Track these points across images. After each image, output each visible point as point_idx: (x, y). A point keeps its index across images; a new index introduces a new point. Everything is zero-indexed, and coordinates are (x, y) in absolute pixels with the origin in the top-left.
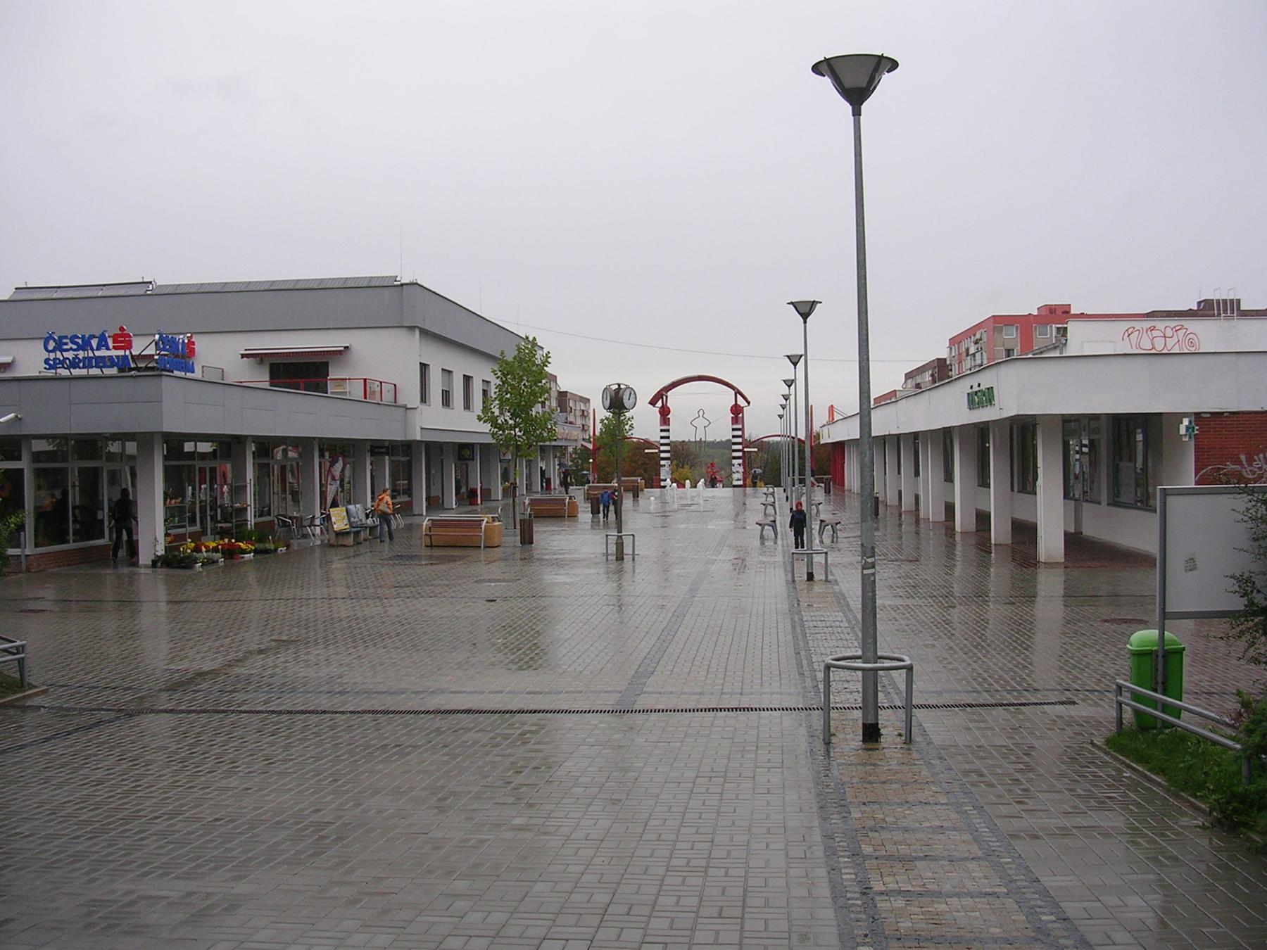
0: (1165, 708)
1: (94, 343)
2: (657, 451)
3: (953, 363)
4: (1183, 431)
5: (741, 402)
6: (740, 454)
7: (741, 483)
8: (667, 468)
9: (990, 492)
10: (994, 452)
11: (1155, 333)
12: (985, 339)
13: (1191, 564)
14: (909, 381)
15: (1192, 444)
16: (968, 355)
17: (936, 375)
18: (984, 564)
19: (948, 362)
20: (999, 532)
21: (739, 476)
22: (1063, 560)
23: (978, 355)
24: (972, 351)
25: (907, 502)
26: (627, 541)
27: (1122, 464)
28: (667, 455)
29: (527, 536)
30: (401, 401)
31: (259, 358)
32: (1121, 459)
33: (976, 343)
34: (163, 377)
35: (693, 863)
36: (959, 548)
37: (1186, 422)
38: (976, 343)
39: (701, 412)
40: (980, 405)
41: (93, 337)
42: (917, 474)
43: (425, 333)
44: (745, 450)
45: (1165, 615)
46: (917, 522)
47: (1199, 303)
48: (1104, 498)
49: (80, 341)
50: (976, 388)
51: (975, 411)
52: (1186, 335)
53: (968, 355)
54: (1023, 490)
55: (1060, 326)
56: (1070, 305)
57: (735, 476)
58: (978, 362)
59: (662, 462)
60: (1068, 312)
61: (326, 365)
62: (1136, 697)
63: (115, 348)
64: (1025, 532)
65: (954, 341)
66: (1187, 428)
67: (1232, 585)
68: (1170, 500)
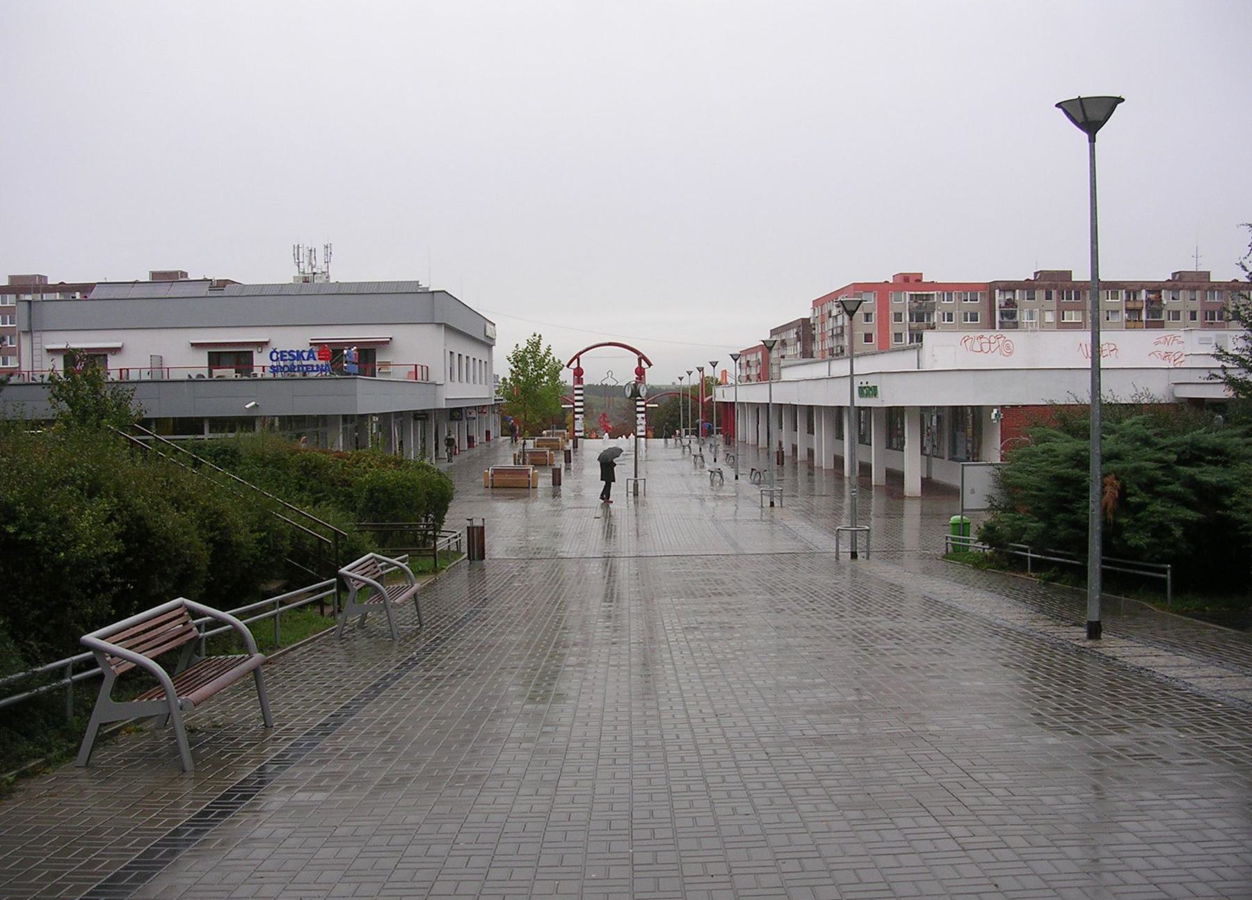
0: (964, 541)
1: (305, 355)
2: (572, 406)
3: (816, 323)
4: (993, 417)
5: (644, 364)
6: (643, 409)
7: (644, 434)
8: (580, 421)
9: (871, 449)
10: (875, 421)
11: (983, 340)
13: (973, 491)
15: (999, 424)
16: (830, 317)
17: (800, 333)
19: (812, 322)
20: (877, 477)
22: (920, 495)
25: (802, 454)
26: (641, 483)
27: (958, 433)
28: (581, 410)
29: (557, 480)
30: (432, 379)
32: (957, 430)
34: (358, 380)
37: (995, 411)
39: (610, 373)
40: (868, 395)
41: (304, 351)
43: (449, 329)
44: (648, 405)
45: (963, 510)
47: (1036, 274)
48: (946, 457)
49: (295, 354)
50: (864, 385)
51: (863, 399)
52: (1004, 342)
53: (830, 317)
54: (889, 446)
55: (913, 293)
56: (921, 274)
57: (639, 428)
58: (840, 323)
59: (577, 416)
60: (919, 281)
62: (953, 539)
63: (320, 359)
64: (895, 478)
65: (817, 303)
66: (996, 415)
67: (985, 498)
68: (965, 468)
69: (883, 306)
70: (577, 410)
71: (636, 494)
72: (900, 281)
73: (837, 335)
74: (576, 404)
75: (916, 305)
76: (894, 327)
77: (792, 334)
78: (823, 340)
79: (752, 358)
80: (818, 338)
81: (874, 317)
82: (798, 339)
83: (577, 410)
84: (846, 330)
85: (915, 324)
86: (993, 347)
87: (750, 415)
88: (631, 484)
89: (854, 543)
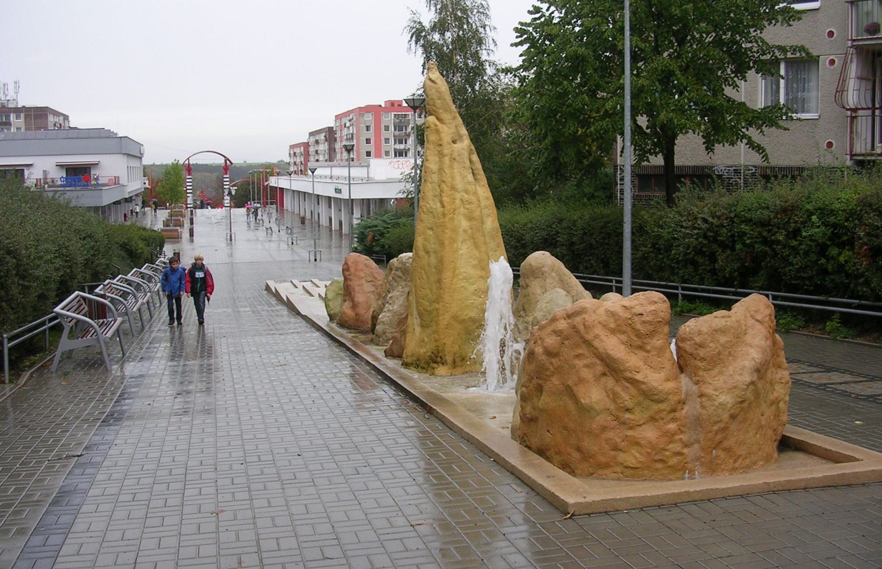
8: (191, 198)
12: (355, 119)
14: (311, 137)
18: (341, 240)
21: (228, 201)
23: (351, 128)
24: (348, 125)
26: (233, 235)
28: (191, 191)
31: (60, 166)
33: (350, 121)
35: (180, 437)
36: (333, 235)
38: (350, 121)
42: (318, 204)
43: (129, 155)
46: (319, 226)
57: (226, 202)
59: (188, 195)
61: (90, 168)
65: (338, 117)
69: (378, 121)
70: (188, 191)
71: (231, 240)
72: (389, 105)
73: (350, 139)
74: (188, 188)
75: (398, 121)
76: (384, 134)
77: (322, 137)
78: (341, 141)
79: (297, 151)
80: (338, 139)
81: (372, 128)
82: (326, 140)
83: (188, 191)
84: (354, 136)
85: (397, 133)
86: (404, 166)
87: (290, 193)
88: (229, 235)
89: (315, 256)
